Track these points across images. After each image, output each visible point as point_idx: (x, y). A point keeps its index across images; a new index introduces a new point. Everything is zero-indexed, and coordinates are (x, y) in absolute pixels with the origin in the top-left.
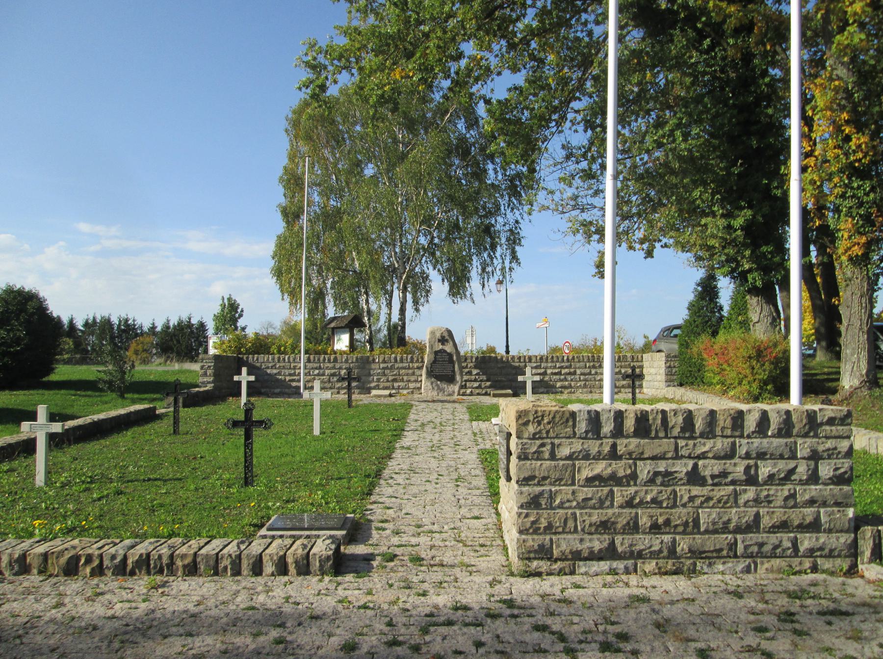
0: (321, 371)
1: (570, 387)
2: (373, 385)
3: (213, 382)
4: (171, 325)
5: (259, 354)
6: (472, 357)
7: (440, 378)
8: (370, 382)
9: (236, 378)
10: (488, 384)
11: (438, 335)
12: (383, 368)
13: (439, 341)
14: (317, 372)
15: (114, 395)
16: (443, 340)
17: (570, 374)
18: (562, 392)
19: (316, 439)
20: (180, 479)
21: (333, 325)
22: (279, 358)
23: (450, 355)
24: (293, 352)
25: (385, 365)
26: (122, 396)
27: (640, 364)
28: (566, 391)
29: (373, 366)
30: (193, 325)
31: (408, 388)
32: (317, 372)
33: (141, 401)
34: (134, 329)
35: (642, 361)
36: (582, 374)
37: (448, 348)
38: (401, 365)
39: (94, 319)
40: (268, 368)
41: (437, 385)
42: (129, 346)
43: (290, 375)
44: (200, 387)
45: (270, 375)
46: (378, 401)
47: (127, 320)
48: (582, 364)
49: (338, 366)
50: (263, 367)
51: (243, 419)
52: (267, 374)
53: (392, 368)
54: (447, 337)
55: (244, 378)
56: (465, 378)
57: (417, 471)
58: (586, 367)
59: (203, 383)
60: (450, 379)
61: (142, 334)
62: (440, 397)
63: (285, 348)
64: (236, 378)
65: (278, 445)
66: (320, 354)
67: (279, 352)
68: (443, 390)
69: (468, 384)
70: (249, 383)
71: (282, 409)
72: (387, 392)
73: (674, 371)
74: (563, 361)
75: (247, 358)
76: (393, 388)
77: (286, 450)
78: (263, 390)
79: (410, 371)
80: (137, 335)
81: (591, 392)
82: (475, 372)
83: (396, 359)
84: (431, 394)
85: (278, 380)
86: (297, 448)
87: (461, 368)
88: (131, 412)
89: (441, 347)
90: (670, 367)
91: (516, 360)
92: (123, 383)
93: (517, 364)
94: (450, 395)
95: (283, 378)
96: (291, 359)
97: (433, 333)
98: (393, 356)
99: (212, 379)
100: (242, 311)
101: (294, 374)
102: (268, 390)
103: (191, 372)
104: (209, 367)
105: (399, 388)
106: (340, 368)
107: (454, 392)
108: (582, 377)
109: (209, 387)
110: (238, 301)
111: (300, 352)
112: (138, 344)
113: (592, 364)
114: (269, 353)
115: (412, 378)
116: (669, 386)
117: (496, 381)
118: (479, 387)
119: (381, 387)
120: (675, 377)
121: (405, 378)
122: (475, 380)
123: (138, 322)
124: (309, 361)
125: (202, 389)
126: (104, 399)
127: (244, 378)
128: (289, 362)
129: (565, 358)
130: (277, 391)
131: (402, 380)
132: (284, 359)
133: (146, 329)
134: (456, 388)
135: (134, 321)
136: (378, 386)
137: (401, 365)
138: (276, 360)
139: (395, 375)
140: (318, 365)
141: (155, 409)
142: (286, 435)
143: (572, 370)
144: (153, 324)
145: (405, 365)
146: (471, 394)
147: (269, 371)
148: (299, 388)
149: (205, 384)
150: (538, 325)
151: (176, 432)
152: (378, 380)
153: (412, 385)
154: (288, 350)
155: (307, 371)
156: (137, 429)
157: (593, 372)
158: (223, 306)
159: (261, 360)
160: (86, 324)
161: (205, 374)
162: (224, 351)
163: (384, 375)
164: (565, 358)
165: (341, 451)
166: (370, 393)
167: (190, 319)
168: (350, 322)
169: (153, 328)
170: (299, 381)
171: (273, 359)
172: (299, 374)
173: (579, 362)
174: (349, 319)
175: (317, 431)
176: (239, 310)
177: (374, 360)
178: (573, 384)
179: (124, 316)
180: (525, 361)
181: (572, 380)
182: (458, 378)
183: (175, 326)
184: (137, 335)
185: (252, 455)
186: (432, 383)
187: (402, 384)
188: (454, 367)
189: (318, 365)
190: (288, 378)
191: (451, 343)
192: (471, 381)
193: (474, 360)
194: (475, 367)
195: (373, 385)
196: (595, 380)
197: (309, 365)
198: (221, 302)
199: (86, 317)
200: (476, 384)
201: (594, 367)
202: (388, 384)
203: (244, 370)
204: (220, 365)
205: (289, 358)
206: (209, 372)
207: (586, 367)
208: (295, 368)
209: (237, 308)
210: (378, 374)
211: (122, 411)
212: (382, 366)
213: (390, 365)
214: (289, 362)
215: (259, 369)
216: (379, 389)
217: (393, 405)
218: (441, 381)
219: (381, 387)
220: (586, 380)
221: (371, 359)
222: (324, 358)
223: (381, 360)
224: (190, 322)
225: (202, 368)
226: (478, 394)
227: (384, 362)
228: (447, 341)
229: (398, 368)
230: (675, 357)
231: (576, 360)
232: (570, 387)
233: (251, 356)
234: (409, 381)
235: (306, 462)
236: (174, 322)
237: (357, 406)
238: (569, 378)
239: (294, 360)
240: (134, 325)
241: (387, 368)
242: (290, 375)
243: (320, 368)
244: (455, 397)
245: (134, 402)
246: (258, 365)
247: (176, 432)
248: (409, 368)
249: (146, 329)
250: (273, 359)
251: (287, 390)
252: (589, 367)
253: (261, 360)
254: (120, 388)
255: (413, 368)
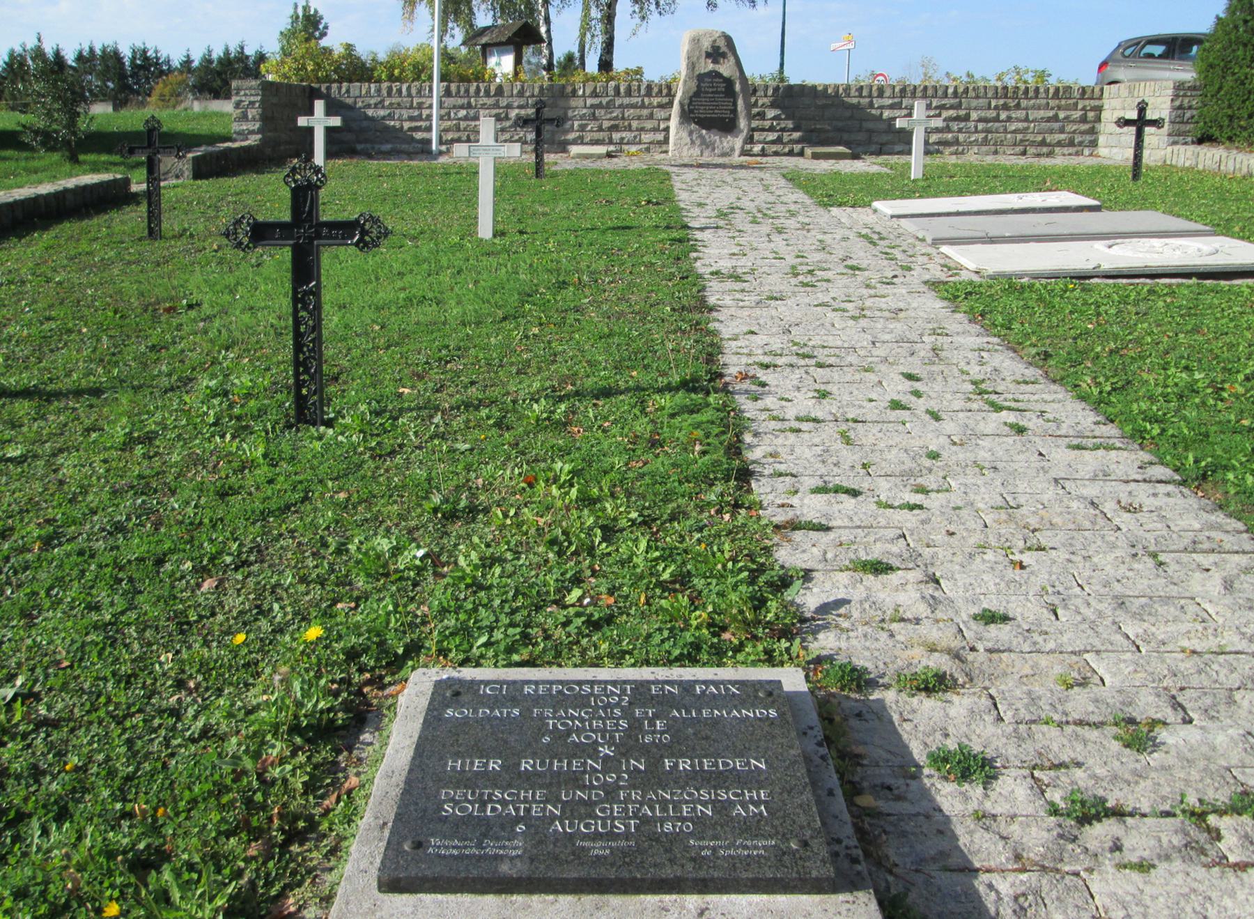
0: (472, 112)
1: (956, 142)
2: (571, 136)
3: (259, 131)
4: (215, 56)
5: (350, 81)
6: (766, 87)
7: (707, 123)
8: (567, 132)
9: (302, 121)
10: (796, 135)
11: (706, 45)
12: (592, 106)
13: (708, 55)
14: (463, 113)
15: (56, 157)
16: (715, 54)
17: (957, 119)
18: (938, 152)
19: (489, 251)
20: (96, 392)
21: (484, 40)
22: (390, 89)
23: (729, 82)
24: (417, 78)
25: (596, 101)
26: (74, 159)
27: (1097, 103)
28: (947, 151)
29: (573, 103)
30: (247, 57)
31: (640, 143)
32: (463, 113)
33: (106, 167)
34: (157, 64)
35: (1100, 98)
36: (980, 120)
37: (726, 69)
38: (627, 101)
39: (92, 50)
40: (369, 106)
41: (701, 137)
42: (151, 89)
43: (411, 119)
44: (234, 141)
45: (372, 119)
46: (588, 164)
47: (145, 52)
48: (983, 102)
49: (503, 102)
50: (360, 104)
51: (286, 217)
52: (367, 118)
53: (609, 106)
54: (724, 49)
55: (319, 121)
56: (755, 124)
57: (821, 355)
58: (989, 108)
59: (239, 133)
60: (727, 126)
61: (170, 71)
62: (706, 159)
63: (403, 71)
64: (302, 121)
65: (397, 266)
66: (469, 81)
67: (391, 78)
68: (706, 144)
69: (757, 136)
70: (329, 131)
71: (399, 181)
72: (602, 150)
73: (1188, 114)
74: (945, 95)
75: (329, 89)
76: (611, 142)
77: (418, 283)
78: (359, 147)
79: (645, 112)
80: (162, 73)
81: (996, 153)
82: (771, 113)
83: (617, 89)
84: (692, 153)
85: (387, 128)
86: (446, 278)
87: (749, 106)
88: (66, 191)
89: (711, 66)
90: (1180, 107)
91: (853, 93)
92: (74, 133)
93: (855, 101)
94: (724, 155)
95: (397, 124)
96: (414, 91)
97: (696, 41)
98: (612, 84)
99: (257, 125)
100: (326, 27)
101: (419, 118)
102: (368, 146)
103: (221, 115)
104: (252, 103)
105: (622, 141)
106: (509, 107)
107: (733, 149)
108: (981, 126)
109: (253, 140)
110: (321, 12)
111: (431, 78)
112: (166, 86)
113: (1001, 102)
114: (369, 80)
115: (649, 125)
116: (1175, 143)
117: (812, 131)
118: (779, 141)
119: (587, 140)
120: (1188, 127)
121: (635, 124)
122: (771, 129)
123: (163, 55)
124: (448, 93)
125: (236, 145)
126: (36, 164)
127: (319, 121)
128: (409, 95)
129: (950, 91)
130: (388, 147)
131: (629, 128)
132: (400, 91)
133: (176, 63)
134: (738, 142)
135: (156, 52)
136: (581, 138)
137: (627, 101)
138: (384, 92)
139: (616, 118)
140: (465, 101)
141: (127, 182)
142: (414, 238)
143: (962, 113)
144: (188, 56)
145: (634, 100)
146: (763, 153)
147: (370, 112)
148: (429, 141)
149: (243, 135)
150: (833, 46)
151: (153, 232)
152: (582, 128)
153: (646, 137)
154: (409, 74)
155: (443, 112)
156: (69, 227)
157: (1003, 116)
158: (295, 18)
159: (356, 92)
160: (80, 58)
161: (244, 117)
162: (285, 76)
163: (594, 117)
164: (950, 91)
165: (563, 285)
166: (565, 151)
167: (242, 48)
168: (515, 34)
169: (188, 62)
170: (429, 129)
171: (379, 91)
172: (429, 117)
173: (977, 97)
174: (515, 29)
175: (485, 230)
176: (321, 27)
177: (574, 91)
178: (961, 137)
179: (139, 45)
180: (870, 96)
181: (960, 131)
182: (742, 123)
183: (220, 60)
184: (162, 73)
185: (317, 327)
186: (691, 133)
187: (627, 135)
188: (735, 104)
189: (465, 101)
190: (406, 125)
191: (732, 59)
192: (763, 130)
193: (770, 92)
194: (773, 105)
195: (571, 136)
196: (1005, 131)
197: (449, 102)
198: (291, 12)
199: (78, 48)
200: (772, 136)
201: (1006, 107)
202: (601, 135)
203: (319, 105)
204: (275, 100)
205: (409, 88)
206: (251, 113)
207: (989, 108)
208: (420, 106)
209: (319, 22)
210: (582, 117)
211: (45, 189)
212: (589, 102)
213: (605, 101)
214: (409, 95)
215: (351, 108)
216: (582, 143)
217: (625, 173)
218: (708, 128)
219: (587, 140)
220: (988, 131)
221: (569, 89)
222: (478, 89)
223: (588, 92)
224: (242, 52)
225: (237, 105)
226: (776, 154)
227: (594, 94)
228: (724, 55)
229: (620, 106)
230: (1194, 88)
231: (971, 94)
232: (956, 142)
233: (335, 86)
234: (642, 129)
235: (478, 324)
236: (217, 53)
237: (554, 175)
238: (955, 126)
239: (419, 91)
240: (158, 59)
241: (600, 106)
242: (411, 119)
243: (469, 106)
244: (737, 159)
245: (95, 169)
246: (349, 101)
247: (153, 232)
248: (643, 106)
249: (176, 63)
250: (379, 91)
251: (404, 147)
252: (996, 108)
253: (356, 92)
254: (69, 142)
255: (650, 106)
